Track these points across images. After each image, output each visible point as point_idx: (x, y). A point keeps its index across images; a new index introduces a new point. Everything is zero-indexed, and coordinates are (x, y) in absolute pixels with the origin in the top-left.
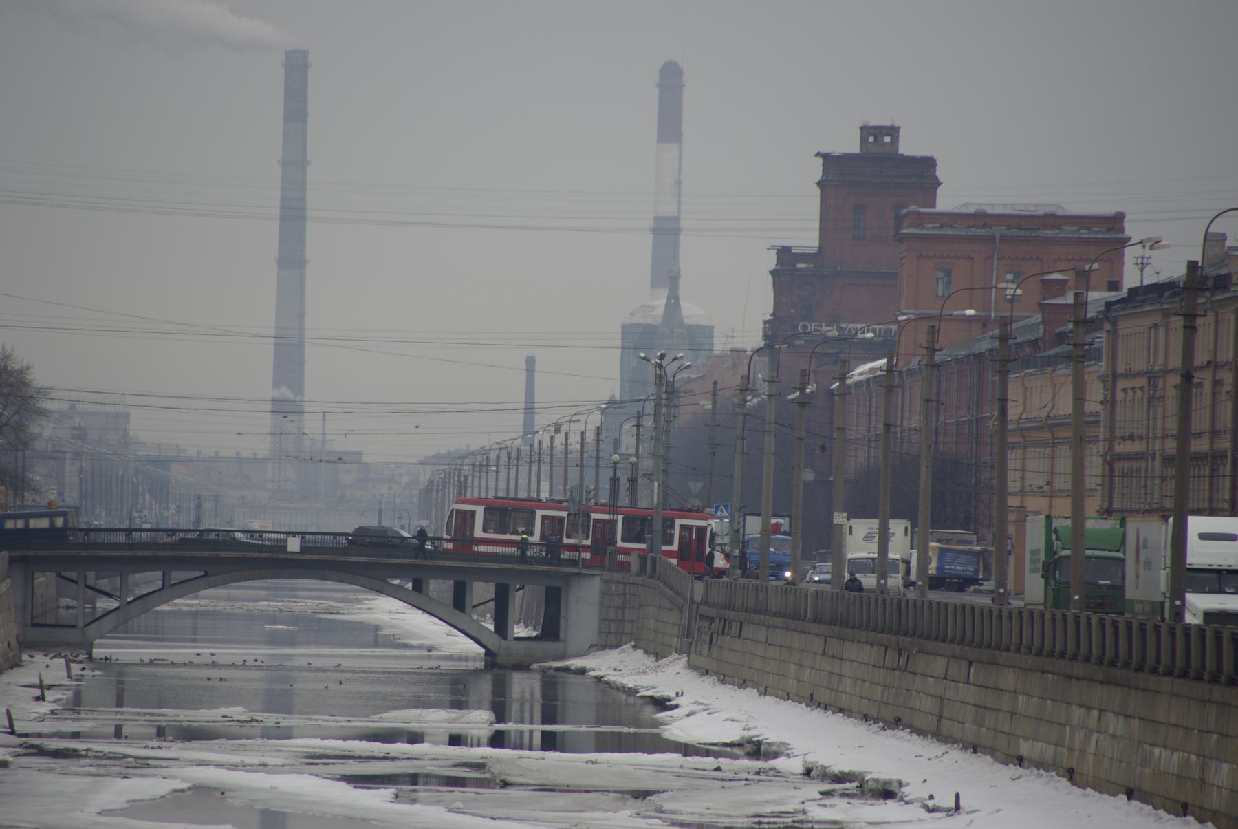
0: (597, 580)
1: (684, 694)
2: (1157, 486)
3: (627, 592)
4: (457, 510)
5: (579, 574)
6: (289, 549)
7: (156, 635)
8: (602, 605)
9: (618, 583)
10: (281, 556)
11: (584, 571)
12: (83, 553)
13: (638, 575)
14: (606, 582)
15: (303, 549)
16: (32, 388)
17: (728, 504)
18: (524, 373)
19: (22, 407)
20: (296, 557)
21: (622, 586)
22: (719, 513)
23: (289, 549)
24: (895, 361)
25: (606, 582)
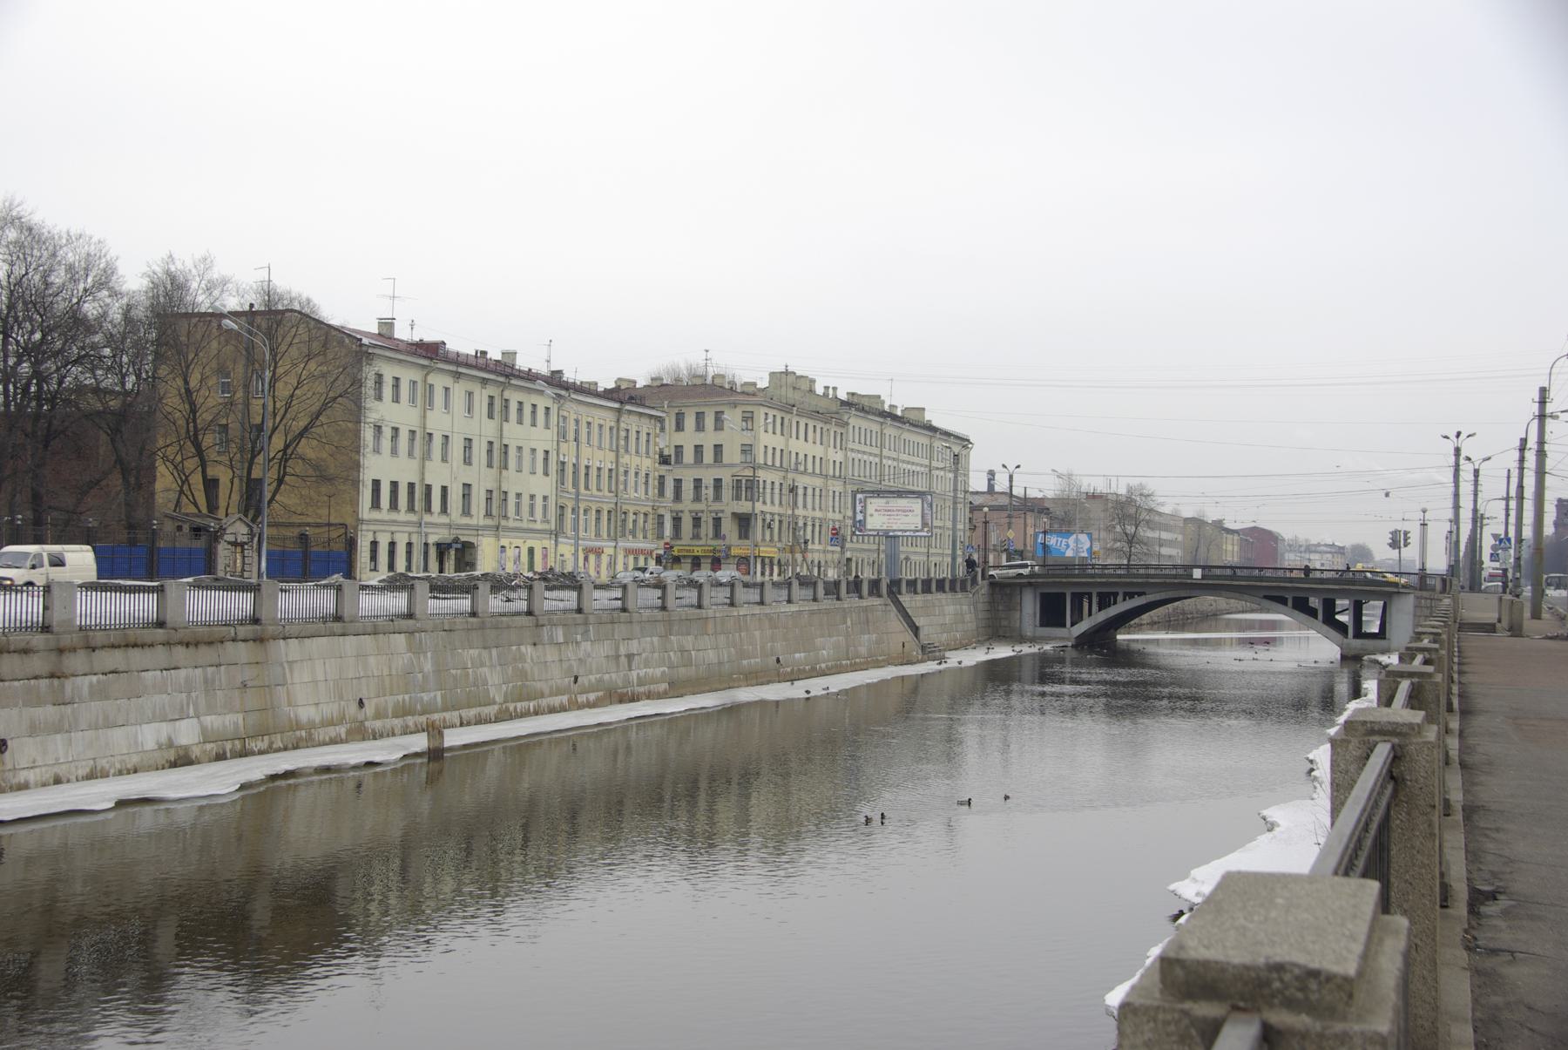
0: (1412, 596)
1: (1456, 434)
2: (19, 396)
3: (1433, 605)
4: (1064, 625)
5: (1399, 592)
6: (1194, 577)
7: (1139, 628)
8: (1415, 615)
9: (1426, 598)
10: (1189, 581)
11: (1401, 590)
12: (1064, 580)
13: (1441, 593)
14: (1418, 598)
15: (1204, 577)
16: (1077, 475)
17: (1545, 576)
18: (1472, 502)
19: (29, 430)
20: (1199, 582)
21: (1429, 601)
22: (1503, 544)
23: (1194, 577)
24: (847, 711)
25: (1418, 598)
